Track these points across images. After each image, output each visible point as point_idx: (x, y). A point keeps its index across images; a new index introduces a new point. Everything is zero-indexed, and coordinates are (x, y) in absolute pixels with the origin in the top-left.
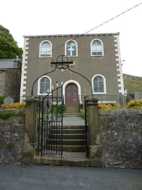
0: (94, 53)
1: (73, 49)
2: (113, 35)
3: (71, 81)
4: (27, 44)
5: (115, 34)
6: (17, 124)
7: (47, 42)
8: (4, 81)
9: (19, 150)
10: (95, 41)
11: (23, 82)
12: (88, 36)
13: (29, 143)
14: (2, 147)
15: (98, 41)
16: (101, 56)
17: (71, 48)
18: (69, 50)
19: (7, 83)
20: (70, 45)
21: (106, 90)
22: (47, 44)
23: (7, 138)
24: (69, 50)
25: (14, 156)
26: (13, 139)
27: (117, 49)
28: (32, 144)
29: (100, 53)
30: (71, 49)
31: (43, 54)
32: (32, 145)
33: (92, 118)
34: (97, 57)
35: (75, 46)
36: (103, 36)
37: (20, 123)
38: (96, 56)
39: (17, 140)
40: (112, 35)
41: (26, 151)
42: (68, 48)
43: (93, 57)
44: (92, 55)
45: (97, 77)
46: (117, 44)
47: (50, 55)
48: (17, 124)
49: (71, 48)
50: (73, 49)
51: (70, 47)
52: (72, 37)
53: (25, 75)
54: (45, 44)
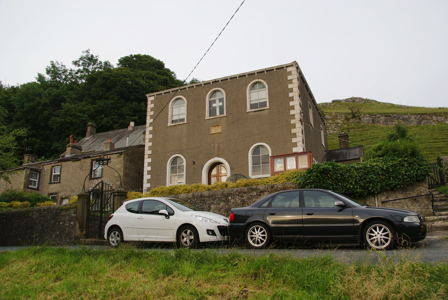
0: (252, 106)
1: (221, 104)
2: (285, 68)
3: (216, 159)
4: (151, 107)
5: (288, 65)
6: (73, 215)
7: (180, 99)
8: (122, 169)
9: (73, 235)
10: (256, 83)
11: (147, 168)
12: (243, 77)
13: (79, 228)
14: (63, 233)
15: (259, 83)
16: (264, 110)
17: (217, 101)
18: (214, 105)
19: (127, 171)
20: (215, 97)
21: (166, 179)
22: (180, 101)
23: (67, 226)
24: (214, 105)
25: (70, 239)
26: (70, 226)
27: (292, 91)
28: (80, 229)
29: (264, 104)
30: (217, 105)
31: (175, 118)
32: (80, 230)
33: (116, 207)
34: (258, 112)
35: (223, 98)
36: (269, 72)
37: (74, 214)
38: (255, 111)
39: (72, 227)
40: (283, 68)
41: (77, 235)
42: (211, 103)
43: (251, 114)
44: (248, 110)
45: (259, 146)
46: (292, 83)
47: (183, 120)
48: (73, 215)
49: (217, 101)
50: (221, 104)
51: (215, 100)
52: (216, 83)
53: (150, 156)
54: (177, 102)
